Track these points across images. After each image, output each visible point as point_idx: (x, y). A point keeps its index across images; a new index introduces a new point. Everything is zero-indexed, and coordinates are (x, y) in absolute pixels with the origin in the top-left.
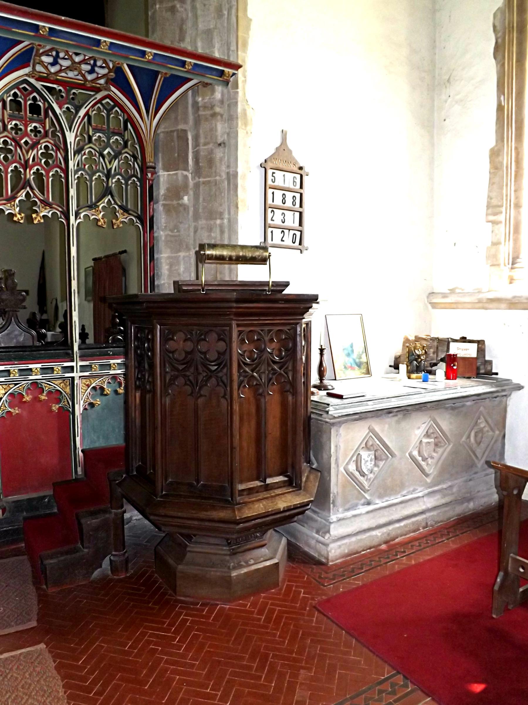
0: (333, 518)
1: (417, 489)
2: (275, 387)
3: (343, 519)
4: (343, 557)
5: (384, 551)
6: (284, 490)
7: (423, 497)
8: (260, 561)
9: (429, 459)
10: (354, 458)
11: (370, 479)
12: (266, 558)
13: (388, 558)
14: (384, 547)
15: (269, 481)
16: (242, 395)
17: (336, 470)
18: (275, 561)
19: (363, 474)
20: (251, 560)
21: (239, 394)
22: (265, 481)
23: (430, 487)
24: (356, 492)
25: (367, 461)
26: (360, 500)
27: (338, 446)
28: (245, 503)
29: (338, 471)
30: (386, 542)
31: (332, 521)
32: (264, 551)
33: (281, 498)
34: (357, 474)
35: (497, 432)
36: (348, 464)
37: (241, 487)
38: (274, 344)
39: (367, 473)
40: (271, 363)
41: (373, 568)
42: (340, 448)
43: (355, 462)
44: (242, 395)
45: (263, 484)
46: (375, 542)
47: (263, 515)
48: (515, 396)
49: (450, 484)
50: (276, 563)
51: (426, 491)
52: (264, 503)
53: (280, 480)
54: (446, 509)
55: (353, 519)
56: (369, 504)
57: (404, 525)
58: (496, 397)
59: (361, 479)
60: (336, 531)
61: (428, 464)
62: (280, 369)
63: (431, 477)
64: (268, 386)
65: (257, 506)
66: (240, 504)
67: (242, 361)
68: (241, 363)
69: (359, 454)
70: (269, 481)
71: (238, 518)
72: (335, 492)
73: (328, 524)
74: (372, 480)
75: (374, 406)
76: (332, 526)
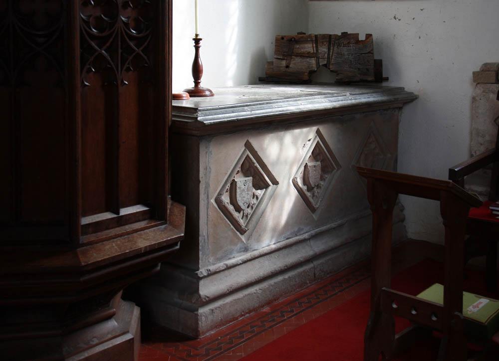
0: (202, 271)
1: (303, 229)
2: (130, 73)
3: (216, 273)
4: (216, 327)
5: (266, 314)
6: (142, 224)
7: (309, 239)
8: (107, 338)
9: (315, 189)
10: (228, 186)
11: (247, 216)
12: (114, 334)
13: (274, 320)
14: (266, 309)
15: (124, 211)
16: (87, 81)
17: (206, 201)
18: (129, 337)
19: (238, 209)
20: (94, 339)
21: (83, 82)
22: (118, 213)
23: (318, 226)
24: (230, 233)
25: (244, 190)
26: (236, 244)
27: (208, 168)
28: (90, 243)
29: (208, 202)
30: (269, 303)
31: (201, 276)
32: (112, 324)
33: (141, 235)
34: (231, 208)
35: (389, 155)
36: (220, 194)
37: (85, 221)
38: (129, 9)
39: (243, 207)
40: (88, 38)
41: (255, 335)
42: (210, 172)
43: (228, 193)
44: (87, 81)
45: (115, 216)
46: (255, 303)
47: (260, 205)
48: (407, 110)
49: (339, 222)
50: (130, 340)
51: (313, 232)
52: (119, 242)
53: (138, 210)
54: (334, 255)
55: (226, 272)
56: (246, 250)
57: (289, 277)
58: (387, 110)
59: (236, 215)
60: (207, 289)
61: (313, 196)
62: (138, 46)
63: (318, 212)
64: (121, 73)
65: (107, 247)
66: (84, 245)
67: (86, 30)
68: (84, 32)
69: (234, 180)
70: (124, 211)
71: (83, 264)
72: (205, 234)
73: (195, 280)
74: (249, 216)
75: (253, 112)
76: (202, 283)
